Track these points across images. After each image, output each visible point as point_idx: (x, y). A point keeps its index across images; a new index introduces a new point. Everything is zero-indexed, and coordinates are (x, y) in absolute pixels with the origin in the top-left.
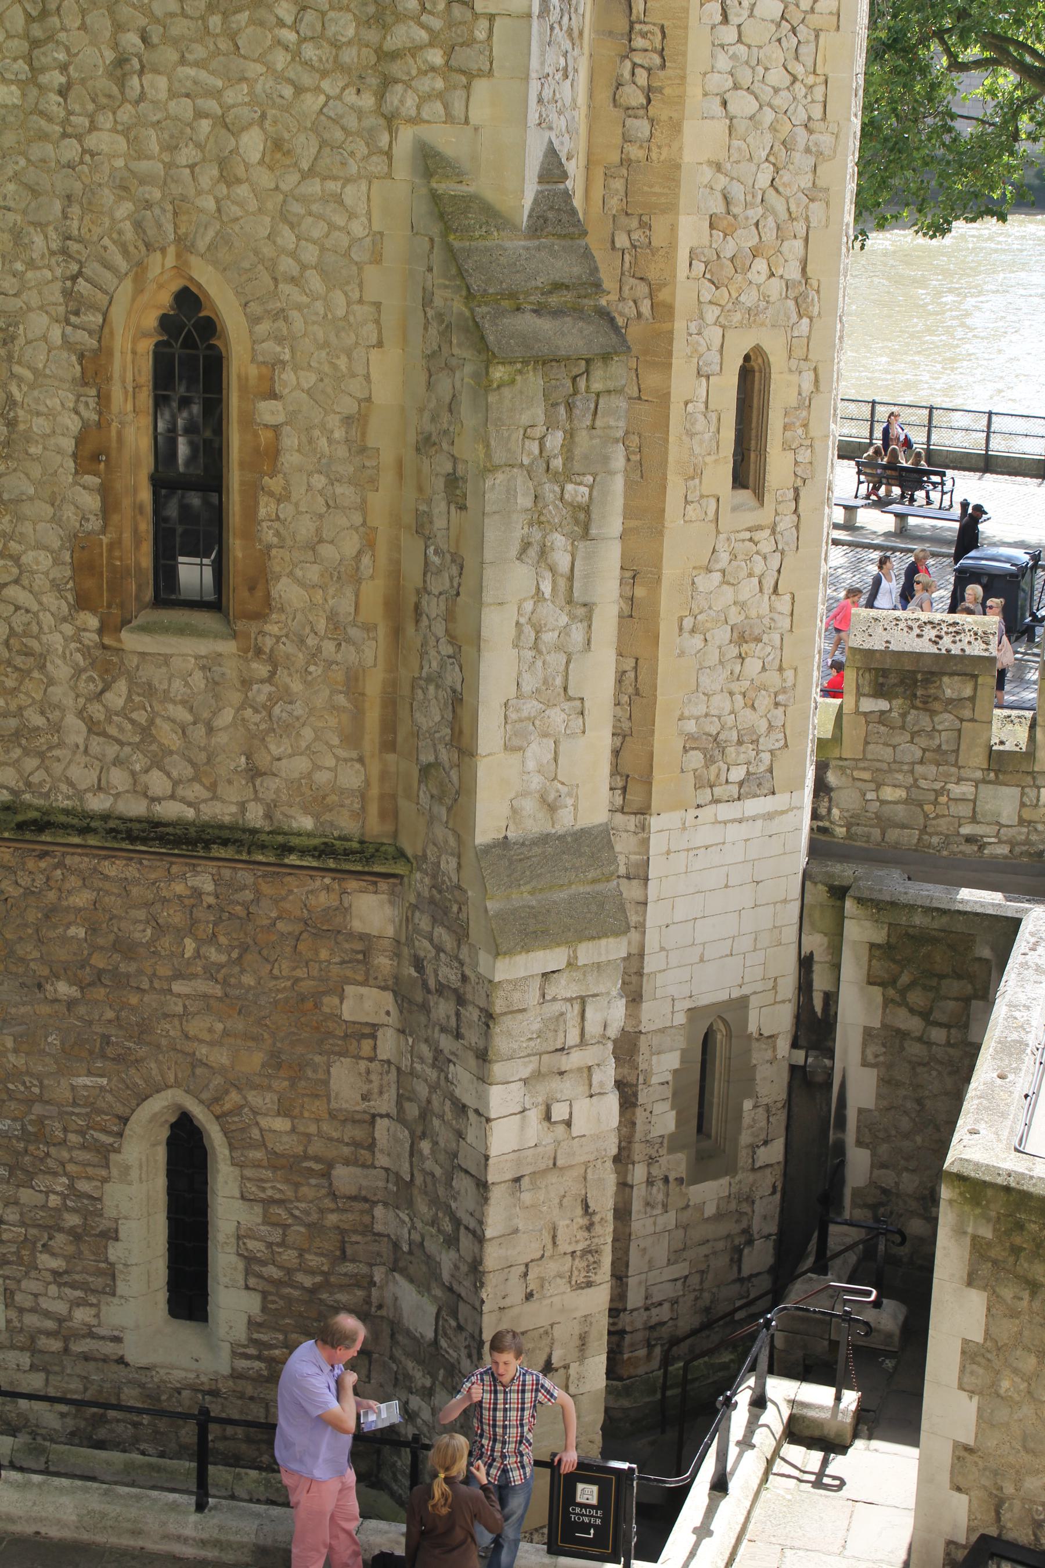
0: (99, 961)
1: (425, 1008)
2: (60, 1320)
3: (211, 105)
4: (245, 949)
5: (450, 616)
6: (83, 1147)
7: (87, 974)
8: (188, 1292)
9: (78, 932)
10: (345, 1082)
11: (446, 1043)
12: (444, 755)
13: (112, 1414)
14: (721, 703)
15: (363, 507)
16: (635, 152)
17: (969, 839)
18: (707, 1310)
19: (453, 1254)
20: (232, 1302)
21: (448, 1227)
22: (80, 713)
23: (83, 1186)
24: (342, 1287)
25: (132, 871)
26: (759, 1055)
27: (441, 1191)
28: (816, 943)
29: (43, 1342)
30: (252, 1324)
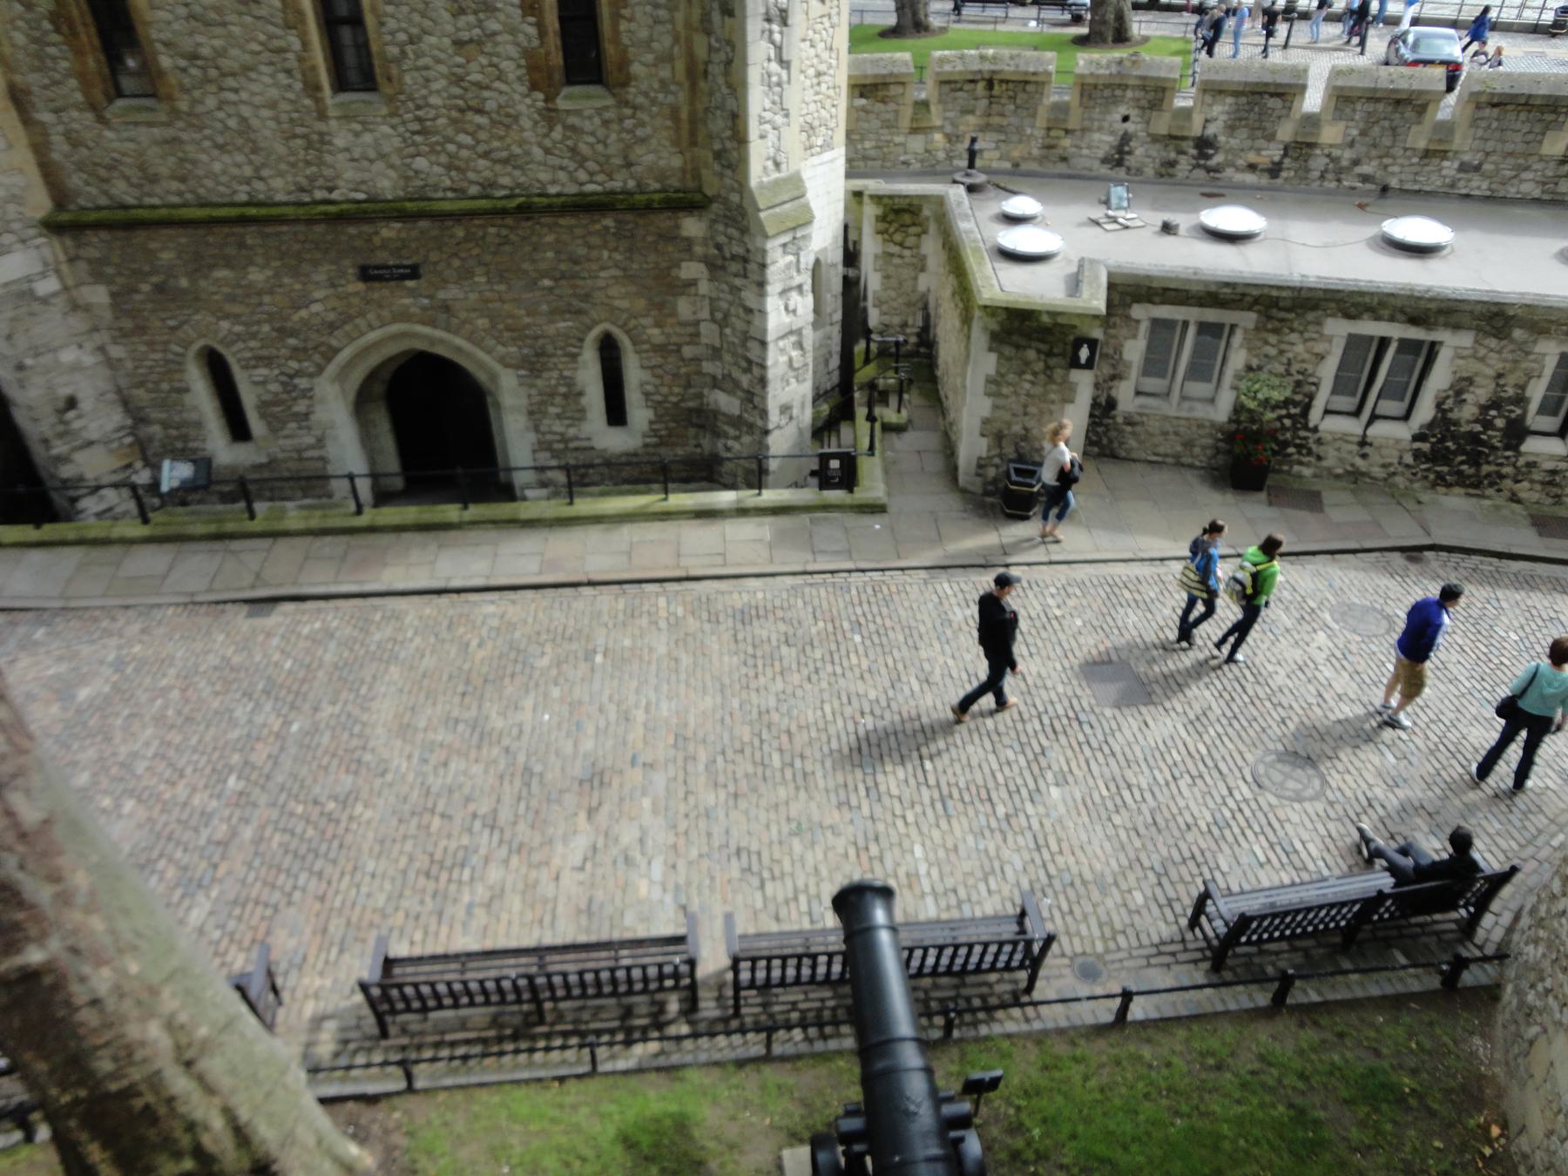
5: (727, 74)
8: (616, 414)
9: (550, 254)
10: (684, 307)
12: (729, 145)
15: (672, 21)
22: (540, 145)
25: (573, 221)
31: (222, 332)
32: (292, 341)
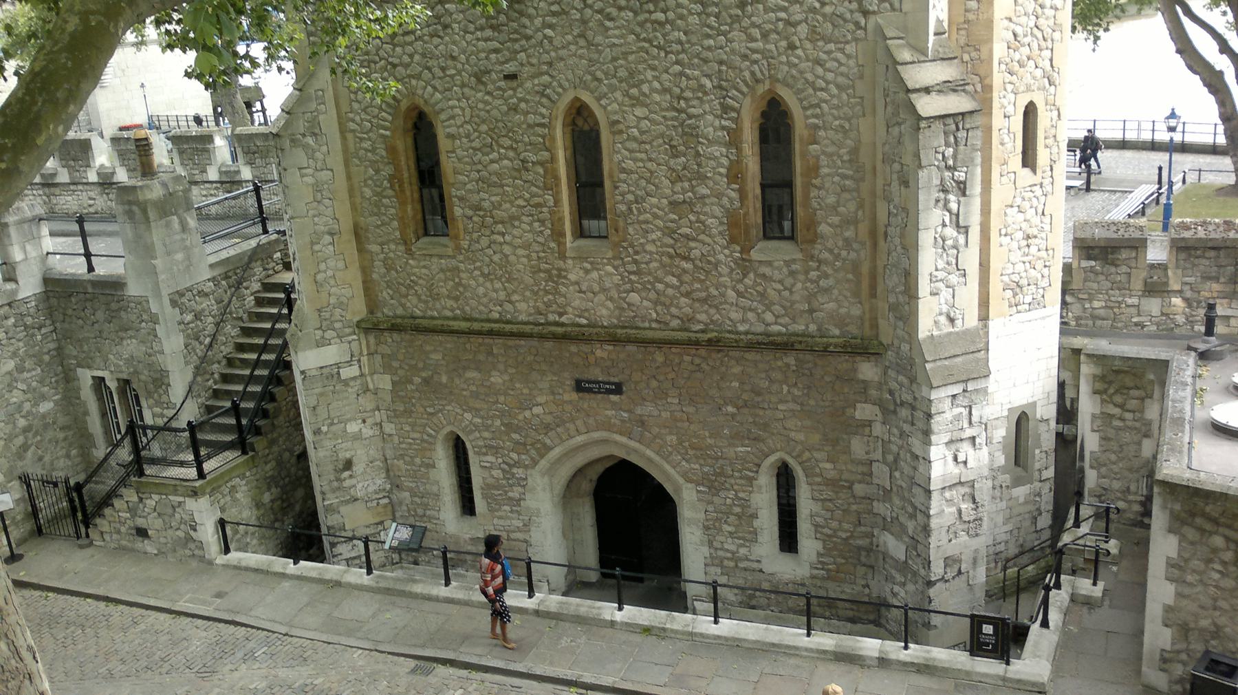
0: (745, 396)
1: (895, 412)
2: (733, 553)
3: (783, 15)
4: (809, 388)
5: (902, 236)
6: (741, 478)
7: (740, 403)
8: (788, 540)
10: (858, 447)
11: (906, 427)
13: (758, 593)
14: (1020, 267)
15: (857, 190)
16: (971, 16)
17: (1136, 324)
18: (1022, 546)
19: (914, 522)
20: (808, 544)
21: (910, 510)
22: (734, 289)
23: (741, 495)
24: (859, 538)
25: (758, 357)
26: (1043, 427)
27: (906, 494)
28: (1067, 376)
29: (726, 563)
30: (819, 555)
31: (465, 422)
32: (515, 436)
